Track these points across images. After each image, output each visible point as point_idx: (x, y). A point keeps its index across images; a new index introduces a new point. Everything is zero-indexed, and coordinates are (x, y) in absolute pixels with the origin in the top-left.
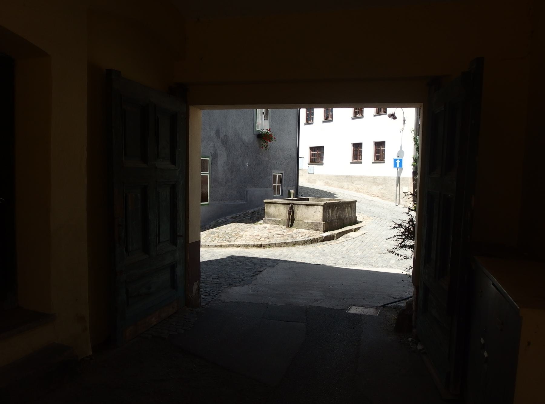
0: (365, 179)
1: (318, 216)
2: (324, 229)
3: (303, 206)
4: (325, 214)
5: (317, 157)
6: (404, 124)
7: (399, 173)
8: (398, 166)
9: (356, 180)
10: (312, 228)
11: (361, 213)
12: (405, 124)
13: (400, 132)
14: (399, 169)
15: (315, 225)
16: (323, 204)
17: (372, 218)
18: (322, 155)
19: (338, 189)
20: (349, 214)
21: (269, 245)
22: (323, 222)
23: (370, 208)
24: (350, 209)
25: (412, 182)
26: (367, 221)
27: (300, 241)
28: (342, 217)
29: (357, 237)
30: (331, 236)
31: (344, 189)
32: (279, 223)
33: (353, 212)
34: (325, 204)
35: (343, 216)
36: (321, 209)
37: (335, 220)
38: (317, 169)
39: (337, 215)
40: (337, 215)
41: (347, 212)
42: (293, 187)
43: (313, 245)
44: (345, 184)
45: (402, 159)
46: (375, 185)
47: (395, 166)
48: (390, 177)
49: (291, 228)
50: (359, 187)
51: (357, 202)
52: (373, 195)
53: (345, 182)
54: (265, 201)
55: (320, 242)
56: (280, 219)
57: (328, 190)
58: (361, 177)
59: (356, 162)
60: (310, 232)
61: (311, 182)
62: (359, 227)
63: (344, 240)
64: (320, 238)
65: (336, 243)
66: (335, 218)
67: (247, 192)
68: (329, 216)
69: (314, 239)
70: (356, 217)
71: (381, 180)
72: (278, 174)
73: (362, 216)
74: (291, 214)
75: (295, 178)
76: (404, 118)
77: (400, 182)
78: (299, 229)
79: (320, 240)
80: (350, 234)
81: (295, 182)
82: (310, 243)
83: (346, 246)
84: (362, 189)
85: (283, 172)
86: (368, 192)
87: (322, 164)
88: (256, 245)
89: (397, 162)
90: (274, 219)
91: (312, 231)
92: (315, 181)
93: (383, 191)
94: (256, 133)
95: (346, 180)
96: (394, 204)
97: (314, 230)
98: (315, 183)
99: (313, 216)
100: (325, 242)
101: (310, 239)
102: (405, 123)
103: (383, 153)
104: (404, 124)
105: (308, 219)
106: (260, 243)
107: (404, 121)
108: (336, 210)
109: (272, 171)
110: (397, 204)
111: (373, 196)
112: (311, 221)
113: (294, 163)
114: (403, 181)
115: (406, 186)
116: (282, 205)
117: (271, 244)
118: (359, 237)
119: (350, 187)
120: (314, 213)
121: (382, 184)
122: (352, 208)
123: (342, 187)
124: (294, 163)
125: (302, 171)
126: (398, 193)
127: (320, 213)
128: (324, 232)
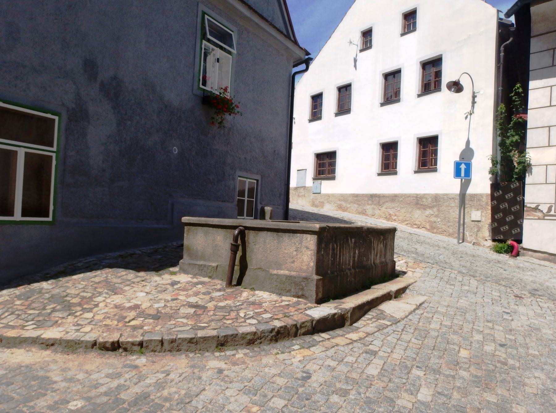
0: (401, 199)
1: (305, 260)
2: (320, 295)
3: (269, 233)
4: (323, 255)
5: (327, 168)
6: (474, 103)
7: (465, 185)
8: (463, 174)
9: (387, 202)
10: (289, 291)
11: (401, 256)
12: (476, 103)
13: (466, 118)
14: (463, 180)
15: (296, 284)
16: (317, 230)
17: (422, 265)
18: (333, 165)
19: (357, 215)
20: (381, 256)
21: (141, 344)
22: (316, 277)
23: (416, 247)
24: (382, 246)
25: (490, 203)
26: (416, 270)
27: (239, 336)
28: (365, 263)
29: (406, 317)
30: (336, 316)
31: (367, 215)
32: (212, 273)
33: (388, 254)
34: (322, 229)
35: (368, 260)
36: (311, 241)
37: (350, 269)
38: (327, 187)
39: (354, 257)
40: (354, 257)
41: (377, 253)
42: (279, 207)
43: (279, 345)
44: (369, 209)
45: (470, 163)
46: (419, 209)
47: (457, 174)
48: (447, 195)
49: (237, 287)
50: (391, 212)
51: (397, 232)
52: (416, 224)
53: (368, 204)
54: (185, 219)
55: (305, 334)
56: (214, 265)
57: (341, 217)
58: (396, 196)
59: (387, 172)
60: (282, 301)
61: (317, 206)
62: (405, 285)
63: (371, 328)
64: (303, 323)
65: (349, 341)
66: (349, 264)
67: (173, 204)
68: (334, 259)
69: (286, 326)
70: (394, 263)
71: (430, 200)
72: (249, 180)
73: (404, 261)
74: (239, 254)
75: (283, 191)
76: (474, 93)
77: (467, 202)
78: (257, 292)
79: (303, 330)
80: (387, 307)
81: (282, 197)
82: (271, 340)
83: (381, 354)
84: (396, 215)
85: (258, 177)
86: (408, 219)
87: (333, 178)
88: (100, 344)
89: (461, 168)
90: (201, 263)
91: (287, 300)
92: (322, 204)
93: (433, 219)
94: (199, 93)
95: (370, 202)
96: (455, 241)
97: (294, 296)
98: (322, 207)
99: (292, 260)
100: (317, 337)
101: (273, 330)
102: (475, 101)
103: (433, 155)
104: (474, 103)
105: (279, 266)
106: (114, 337)
107: (474, 97)
108: (352, 245)
109: (235, 172)
110: (460, 242)
111: (416, 226)
112: (287, 272)
113: (281, 166)
114: (472, 200)
115: (478, 210)
116: (220, 230)
117: (147, 341)
118: (410, 317)
119: (377, 212)
120: (295, 253)
121: (431, 207)
122: (386, 244)
123: (364, 213)
124: (281, 166)
125: (304, 189)
126: (462, 222)
127: (309, 253)
128: (320, 301)
